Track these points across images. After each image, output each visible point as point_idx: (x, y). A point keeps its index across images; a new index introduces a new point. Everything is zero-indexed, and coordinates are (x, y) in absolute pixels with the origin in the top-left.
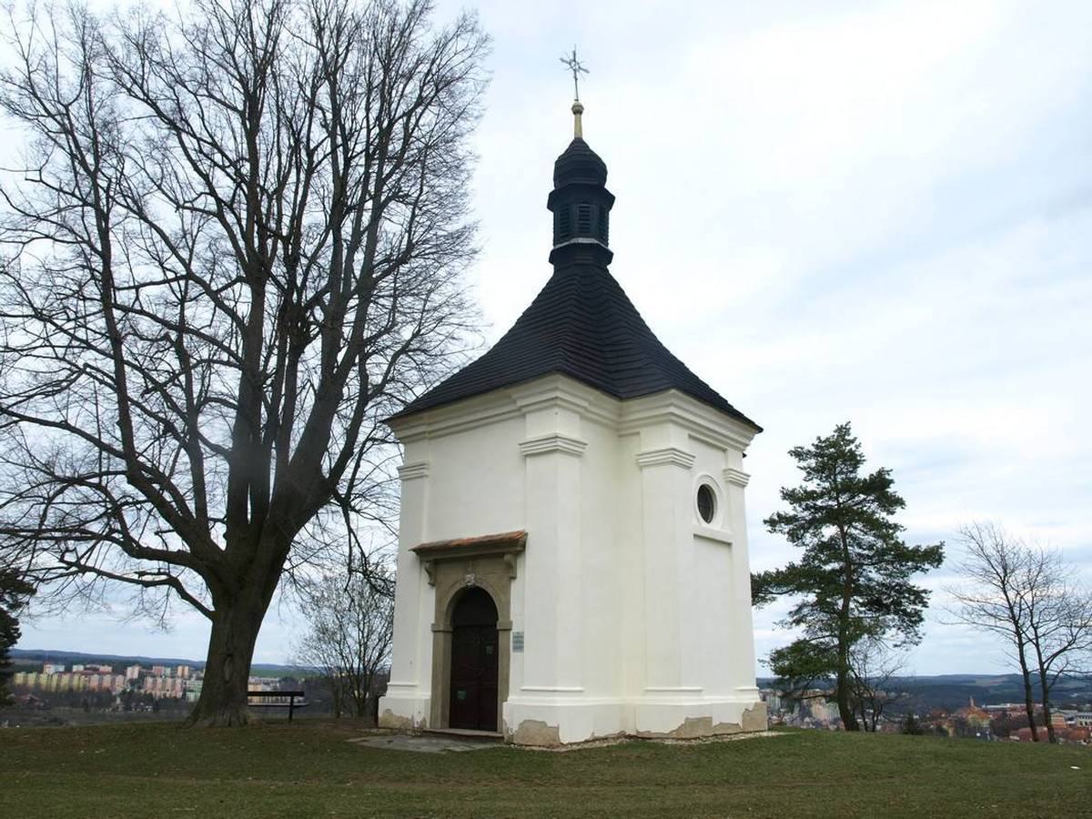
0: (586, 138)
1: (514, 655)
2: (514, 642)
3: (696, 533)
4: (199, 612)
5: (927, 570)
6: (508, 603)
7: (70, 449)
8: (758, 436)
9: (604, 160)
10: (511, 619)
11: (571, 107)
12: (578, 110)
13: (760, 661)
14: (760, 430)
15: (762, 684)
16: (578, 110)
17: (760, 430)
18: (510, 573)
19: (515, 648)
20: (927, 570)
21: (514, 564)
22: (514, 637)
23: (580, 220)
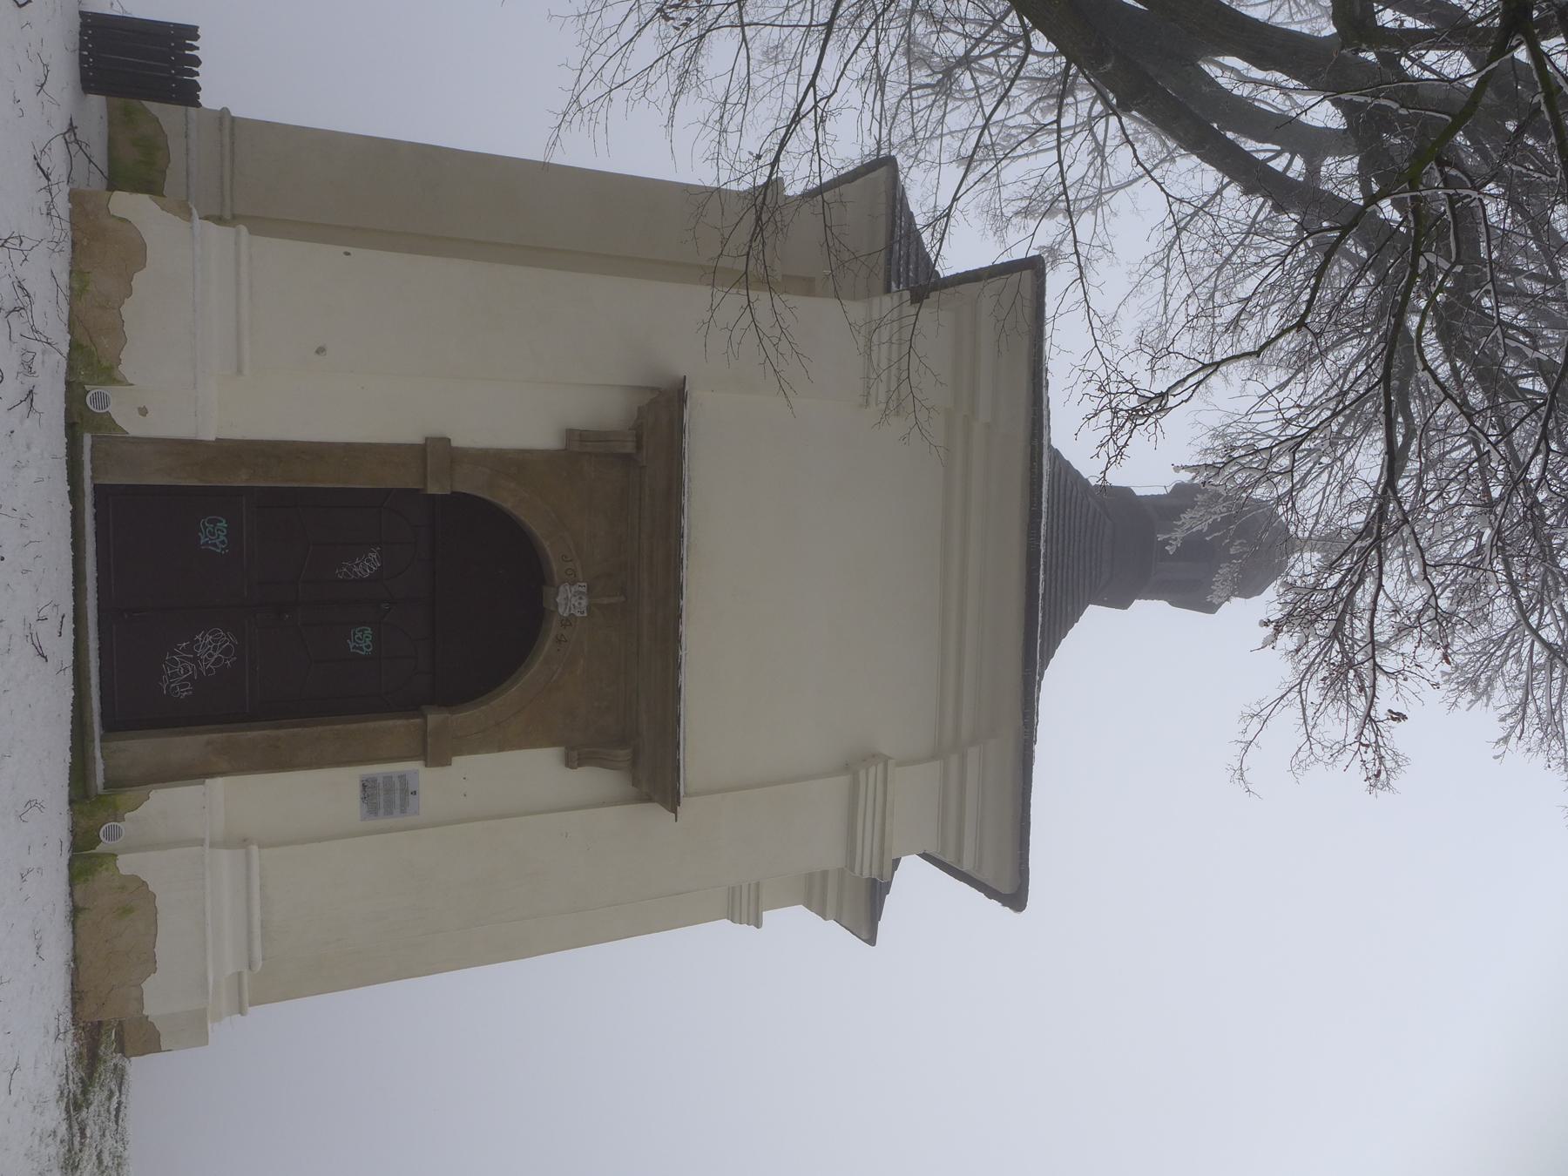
22: (402, 777)
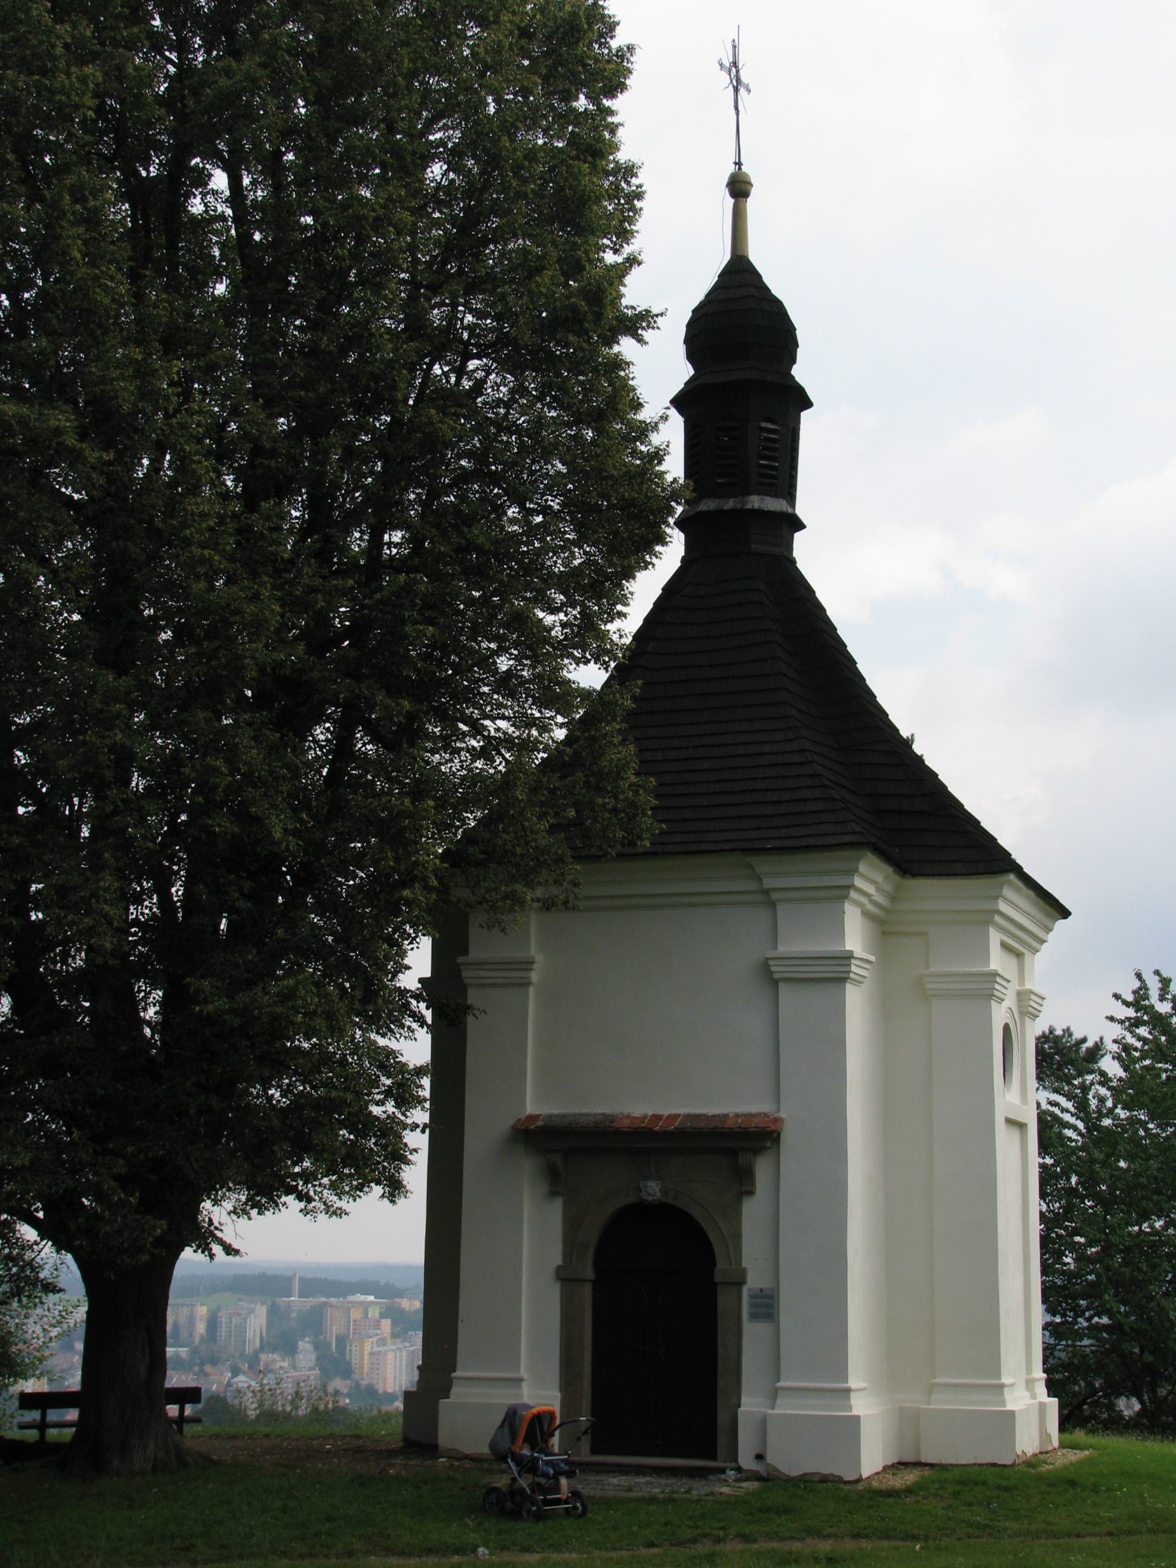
0: (756, 256)
1: (753, 1334)
2: (752, 1306)
3: (1012, 1116)
4: (71, 1409)
5: (1115, 1041)
6: (738, 1236)
7: (380, 1001)
8: (1061, 923)
9: (800, 352)
10: (744, 1265)
11: (725, 180)
12: (739, 188)
13: (1009, 1122)
14: (1065, 913)
15: (618, 344)
16: (739, 188)
17: (1065, 913)
18: (744, 1182)
19: (754, 1316)
20: (1115, 1041)
21: (534, 1411)
22: (751, 1297)
23: (774, 477)
